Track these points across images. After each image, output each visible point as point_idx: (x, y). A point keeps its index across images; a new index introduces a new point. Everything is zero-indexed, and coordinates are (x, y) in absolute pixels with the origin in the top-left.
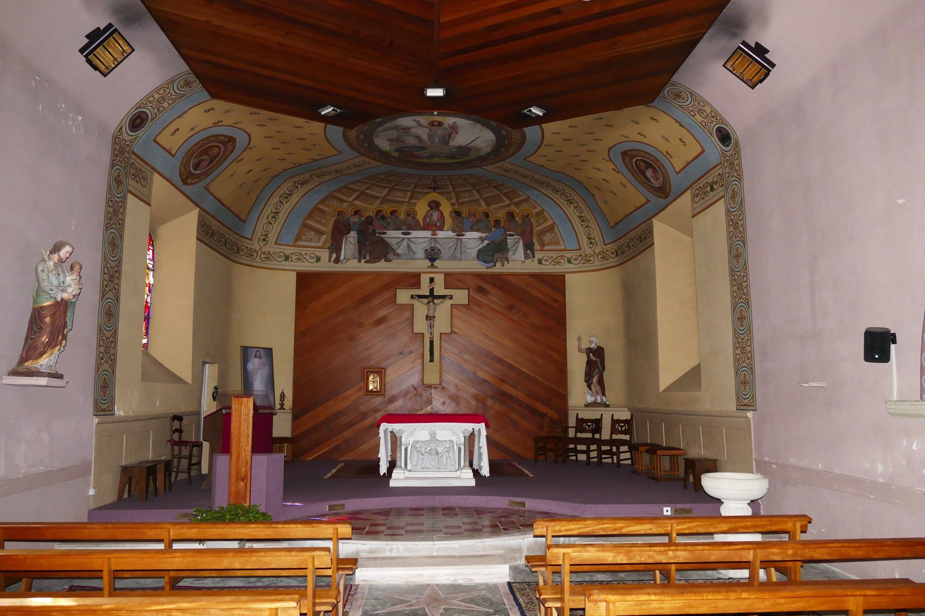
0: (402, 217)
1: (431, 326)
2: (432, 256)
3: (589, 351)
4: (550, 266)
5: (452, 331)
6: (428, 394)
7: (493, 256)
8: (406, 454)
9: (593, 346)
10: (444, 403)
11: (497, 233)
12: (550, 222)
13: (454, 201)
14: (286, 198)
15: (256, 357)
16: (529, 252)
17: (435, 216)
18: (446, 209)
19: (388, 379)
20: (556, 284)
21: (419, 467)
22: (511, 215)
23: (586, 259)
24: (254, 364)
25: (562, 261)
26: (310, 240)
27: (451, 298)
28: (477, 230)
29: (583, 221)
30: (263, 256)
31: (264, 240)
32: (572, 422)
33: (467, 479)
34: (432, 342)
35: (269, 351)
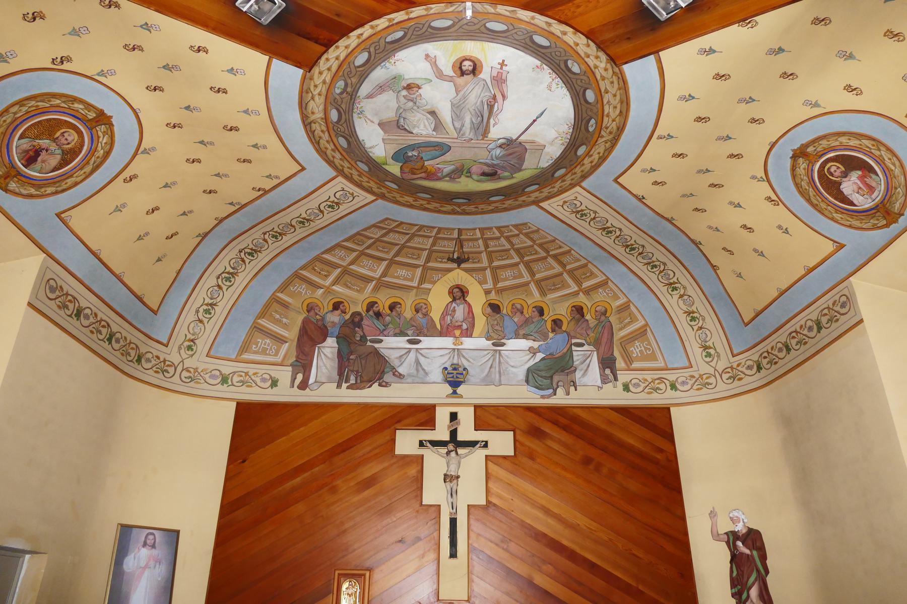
0: (408, 313)
1: (453, 493)
2: (455, 378)
3: (732, 538)
4: (643, 395)
5: (488, 502)
7: (551, 377)
9: (740, 528)
11: (557, 342)
12: (640, 323)
13: (490, 285)
14: (228, 279)
16: (608, 371)
17: (460, 312)
18: (477, 299)
19: (376, 590)
20: (657, 423)
22: (579, 311)
23: (703, 382)
25: (662, 386)
26: (264, 352)
27: (486, 445)
28: (525, 337)
29: (693, 319)
30: (185, 374)
31: (189, 348)
34: (453, 522)
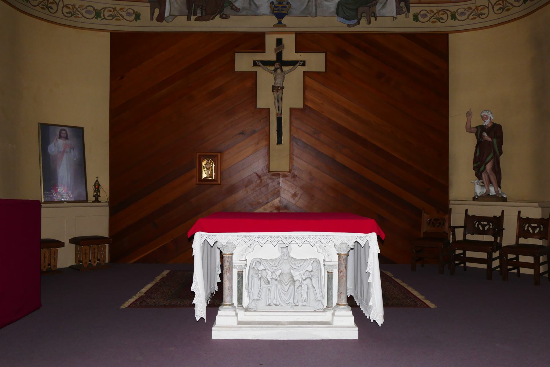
1: (279, 100)
3: (480, 131)
6: (275, 183)
8: (240, 282)
9: (487, 123)
10: (295, 195)
15: (60, 137)
16: (402, 4)
21: (262, 305)
24: (57, 146)
25: (445, 17)
30: (66, 10)
32: (457, 218)
33: (343, 327)
34: (279, 120)
35: (79, 132)
